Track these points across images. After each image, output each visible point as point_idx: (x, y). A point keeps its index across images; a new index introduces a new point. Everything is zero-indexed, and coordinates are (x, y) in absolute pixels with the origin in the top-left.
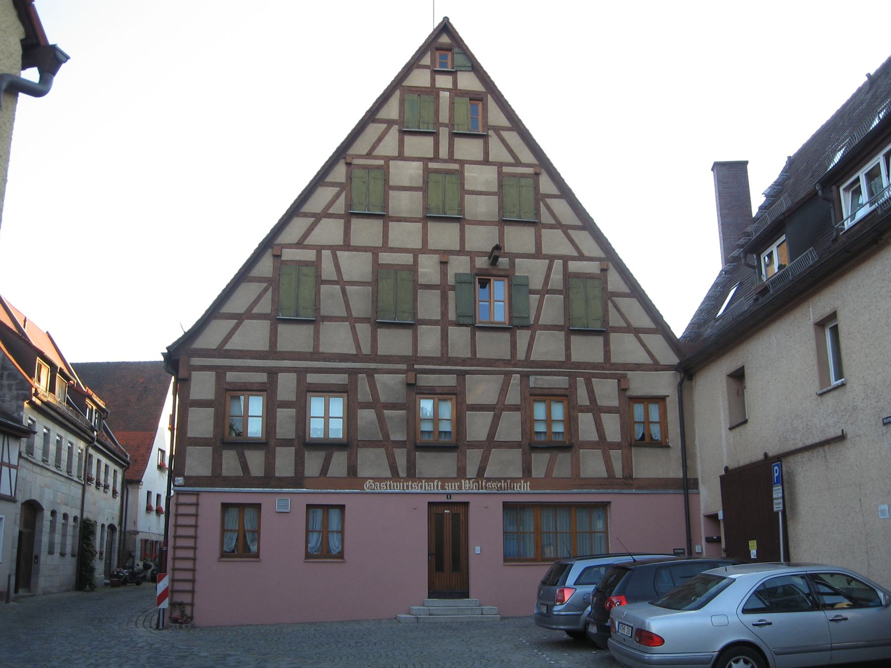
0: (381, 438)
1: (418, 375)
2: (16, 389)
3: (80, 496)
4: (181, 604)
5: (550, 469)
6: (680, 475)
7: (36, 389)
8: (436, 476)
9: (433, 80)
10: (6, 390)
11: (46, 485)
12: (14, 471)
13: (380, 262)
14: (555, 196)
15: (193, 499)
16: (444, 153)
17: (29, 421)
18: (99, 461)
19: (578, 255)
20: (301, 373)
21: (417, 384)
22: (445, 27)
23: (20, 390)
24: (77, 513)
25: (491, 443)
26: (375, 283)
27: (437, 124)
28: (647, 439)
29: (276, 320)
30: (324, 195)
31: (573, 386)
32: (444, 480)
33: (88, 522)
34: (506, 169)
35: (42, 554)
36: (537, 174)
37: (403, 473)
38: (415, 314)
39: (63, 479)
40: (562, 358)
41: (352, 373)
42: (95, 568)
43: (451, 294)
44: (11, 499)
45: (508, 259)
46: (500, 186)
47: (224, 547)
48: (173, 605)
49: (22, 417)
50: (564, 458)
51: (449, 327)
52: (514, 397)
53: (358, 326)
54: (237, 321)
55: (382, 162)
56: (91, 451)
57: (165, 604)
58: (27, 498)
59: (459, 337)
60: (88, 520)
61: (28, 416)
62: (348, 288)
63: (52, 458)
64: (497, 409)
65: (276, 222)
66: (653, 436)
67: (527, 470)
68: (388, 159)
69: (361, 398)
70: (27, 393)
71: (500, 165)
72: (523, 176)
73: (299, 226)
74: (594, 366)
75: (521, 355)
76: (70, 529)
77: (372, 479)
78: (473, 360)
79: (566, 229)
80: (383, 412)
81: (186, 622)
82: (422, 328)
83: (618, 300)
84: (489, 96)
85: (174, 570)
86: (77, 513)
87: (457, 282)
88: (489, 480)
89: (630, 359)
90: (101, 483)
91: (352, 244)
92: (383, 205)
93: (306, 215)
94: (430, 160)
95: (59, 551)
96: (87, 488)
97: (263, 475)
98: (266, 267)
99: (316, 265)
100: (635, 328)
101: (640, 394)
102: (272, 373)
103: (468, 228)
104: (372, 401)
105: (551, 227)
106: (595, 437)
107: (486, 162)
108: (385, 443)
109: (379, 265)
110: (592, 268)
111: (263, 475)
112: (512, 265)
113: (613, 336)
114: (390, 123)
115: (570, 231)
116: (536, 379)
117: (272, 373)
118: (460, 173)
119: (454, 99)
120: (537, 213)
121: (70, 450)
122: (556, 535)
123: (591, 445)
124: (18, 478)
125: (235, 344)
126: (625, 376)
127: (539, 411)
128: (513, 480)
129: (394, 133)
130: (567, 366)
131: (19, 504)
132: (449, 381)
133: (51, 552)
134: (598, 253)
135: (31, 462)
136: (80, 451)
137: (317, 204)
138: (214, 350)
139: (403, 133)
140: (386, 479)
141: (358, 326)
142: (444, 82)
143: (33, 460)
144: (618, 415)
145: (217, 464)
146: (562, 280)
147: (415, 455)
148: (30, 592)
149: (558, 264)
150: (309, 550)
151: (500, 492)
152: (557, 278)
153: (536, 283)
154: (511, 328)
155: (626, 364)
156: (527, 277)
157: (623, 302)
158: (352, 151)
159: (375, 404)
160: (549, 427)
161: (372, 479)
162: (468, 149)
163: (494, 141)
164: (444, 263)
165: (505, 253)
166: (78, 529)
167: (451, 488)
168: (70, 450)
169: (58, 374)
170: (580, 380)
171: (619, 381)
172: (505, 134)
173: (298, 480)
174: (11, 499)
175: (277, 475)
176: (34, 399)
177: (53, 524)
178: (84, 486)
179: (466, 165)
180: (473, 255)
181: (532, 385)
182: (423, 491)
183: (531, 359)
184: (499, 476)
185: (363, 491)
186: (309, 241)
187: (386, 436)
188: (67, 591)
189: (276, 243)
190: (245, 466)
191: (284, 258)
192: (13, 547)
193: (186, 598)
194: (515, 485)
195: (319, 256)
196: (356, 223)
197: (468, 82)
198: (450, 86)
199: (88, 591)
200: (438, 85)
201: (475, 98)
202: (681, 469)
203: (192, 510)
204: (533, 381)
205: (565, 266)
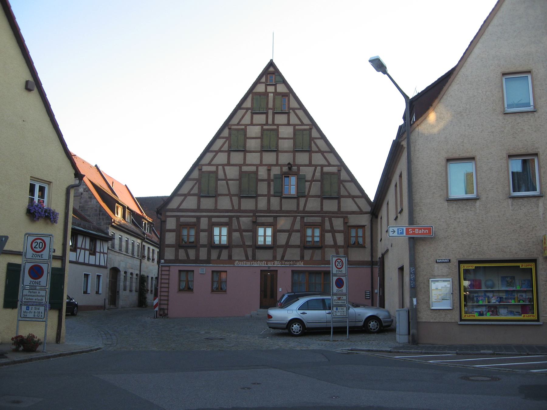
0: (241, 243)
1: (257, 218)
2: (106, 220)
3: (139, 265)
4: (163, 309)
5: (312, 257)
6: (370, 259)
7: (114, 220)
8: (264, 259)
9: (266, 89)
10: (101, 220)
11: (121, 261)
12: (106, 255)
13: (242, 171)
14: (318, 138)
15: (167, 268)
16: (270, 121)
17: (112, 233)
18: (149, 248)
19: (328, 164)
20: (210, 217)
21: (257, 222)
22: (271, 64)
23: (107, 220)
24: (138, 272)
25: (287, 246)
26: (240, 179)
27: (268, 109)
28: (356, 244)
29: (200, 196)
30: (220, 142)
31: (323, 222)
32: (267, 261)
33: (143, 276)
34: (297, 127)
35: (120, 290)
36: (311, 129)
37: (250, 258)
38: (256, 192)
39: (130, 257)
40: (319, 210)
41: (230, 217)
42: (146, 297)
43: (272, 183)
44: (105, 267)
45: (297, 167)
46: (294, 134)
47: (181, 287)
48: (160, 309)
49: (108, 232)
50: (318, 252)
51: (271, 197)
52: (297, 226)
53: (233, 198)
54: (184, 197)
55: (243, 127)
56: (144, 243)
57: (157, 309)
58: (112, 266)
59: (275, 201)
60: (143, 275)
61: (111, 231)
62: (229, 182)
63: (124, 248)
64: (290, 232)
65: (199, 155)
66: (360, 242)
67: (302, 257)
68: (246, 125)
69: (234, 227)
70: (110, 221)
71: (295, 125)
72: (305, 130)
73: (209, 156)
74: (333, 213)
75: (301, 208)
76: (134, 280)
78: (281, 211)
79: (322, 153)
80: (242, 234)
81: (165, 316)
82: (259, 198)
83: (345, 184)
84: (291, 94)
85: (160, 296)
86: (138, 272)
87: (274, 178)
88: (286, 261)
89: (349, 209)
90: (150, 258)
91: (231, 163)
92: (244, 146)
93: (212, 151)
94: (264, 125)
95: (129, 289)
96: (143, 261)
97: (195, 259)
98: (195, 175)
99: (216, 172)
100: (352, 196)
101: (353, 225)
102: (198, 218)
103: (280, 154)
104: (238, 229)
105: (316, 152)
106: (332, 243)
107: (288, 124)
108: (243, 246)
109: (242, 171)
110: (334, 169)
111: (195, 259)
112: (299, 170)
113: (342, 200)
114: (247, 109)
115: (325, 154)
116: (307, 219)
117: (198, 218)
118: (277, 130)
119: (275, 97)
120: (310, 146)
121: (133, 244)
122: (163, 283)
123: (330, 247)
124: (108, 258)
125: (184, 206)
126: (347, 217)
127: (309, 232)
128: (296, 261)
129: (249, 113)
130: (321, 213)
131: (109, 269)
132: (271, 220)
133: (125, 289)
134: (337, 163)
135: (113, 251)
136: (138, 244)
137: (216, 147)
138: (175, 209)
139: (253, 114)
140: (244, 260)
141: (233, 198)
142: (271, 89)
143: (114, 250)
144: (343, 234)
145: (177, 255)
146: (320, 176)
147: (256, 251)
148: (115, 306)
149: (319, 168)
150: (213, 288)
151: (291, 266)
152: (318, 175)
153: (309, 177)
154: (297, 198)
155: (348, 211)
156: (305, 175)
157: (347, 185)
158: (231, 123)
159: (240, 230)
160: (313, 239)
162: (281, 119)
163: (292, 115)
164: (269, 170)
165: (295, 165)
166: (139, 279)
167: (270, 264)
168: (133, 244)
169: (127, 209)
170: (327, 219)
171: (344, 219)
172: (297, 111)
173: (208, 261)
174: (105, 267)
175: (200, 259)
176: (113, 224)
177: (125, 277)
178: (141, 260)
179: (279, 126)
180: (281, 166)
181: (305, 221)
182: (259, 265)
183: (306, 210)
184: (290, 259)
185: (234, 265)
186: (213, 163)
187: (244, 243)
188: (134, 307)
189: (200, 164)
190: (187, 255)
191: (203, 170)
192: (106, 288)
193: (165, 307)
194: (297, 263)
195: (217, 169)
196: (232, 154)
197: (281, 88)
198: (274, 91)
199: (144, 308)
200: (268, 91)
201: (284, 95)
202: (370, 257)
203: (167, 273)
204: (306, 220)
205: (322, 169)
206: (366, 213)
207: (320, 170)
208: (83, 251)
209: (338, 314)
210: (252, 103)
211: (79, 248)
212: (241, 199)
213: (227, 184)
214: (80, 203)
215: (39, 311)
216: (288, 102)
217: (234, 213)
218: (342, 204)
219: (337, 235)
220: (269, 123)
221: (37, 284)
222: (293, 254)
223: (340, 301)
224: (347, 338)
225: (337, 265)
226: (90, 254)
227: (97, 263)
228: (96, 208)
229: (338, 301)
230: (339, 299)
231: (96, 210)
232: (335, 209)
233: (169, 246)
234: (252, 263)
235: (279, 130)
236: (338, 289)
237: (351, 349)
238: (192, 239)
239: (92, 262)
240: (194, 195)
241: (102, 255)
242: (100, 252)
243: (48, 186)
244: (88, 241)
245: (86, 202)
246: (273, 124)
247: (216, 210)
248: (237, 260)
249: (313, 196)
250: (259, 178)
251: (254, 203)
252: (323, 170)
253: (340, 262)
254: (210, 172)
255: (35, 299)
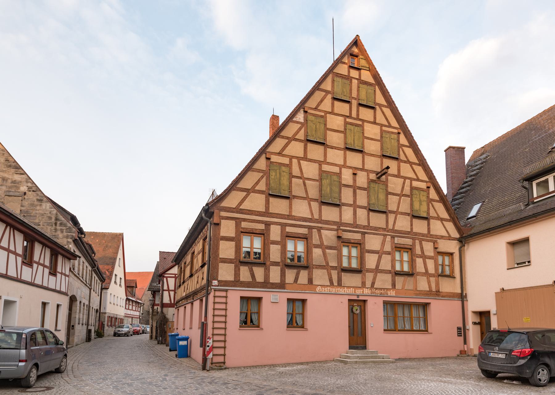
5: (404, 285)
10: (59, 232)
12: (67, 278)
15: (224, 294)
16: (354, 114)
25: (377, 270)
34: (384, 128)
37: (335, 284)
41: (310, 228)
52: (388, 247)
55: (323, 114)
62: (307, 182)
67: (394, 285)
68: (327, 112)
71: (382, 125)
74: (423, 235)
75: (390, 227)
78: (368, 227)
82: (344, 208)
97: (263, 281)
99: (289, 166)
105: (405, 162)
106: (423, 270)
107: (374, 123)
108: (326, 267)
113: (432, 221)
116: (398, 239)
118: (362, 126)
145: (237, 273)
149: (408, 181)
167: (359, 292)
174: (65, 294)
175: (271, 281)
181: (396, 242)
184: (381, 287)
185: (315, 292)
187: (327, 263)
204: (397, 240)
206: (454, 239)
207: (409, 184)
208: (41, 268)
210: (333, 86)
211: (36, 263)
212: (322, 206)
213: (305, 184)
214: (22, 206)
222: (384, 281)
226: (50, 273)
227: (58, 289)
228: (49, 215)
231: (50, 218)
233: (225, 261)
234: (338, 290)
239: (52, 286)
241: (63, 277)
242: (62, 273)
244: (48, 253)
245: (32, 205)
247: (289, 217)
248: (319, 285)
249: (402, 214)
251: (338, 213)
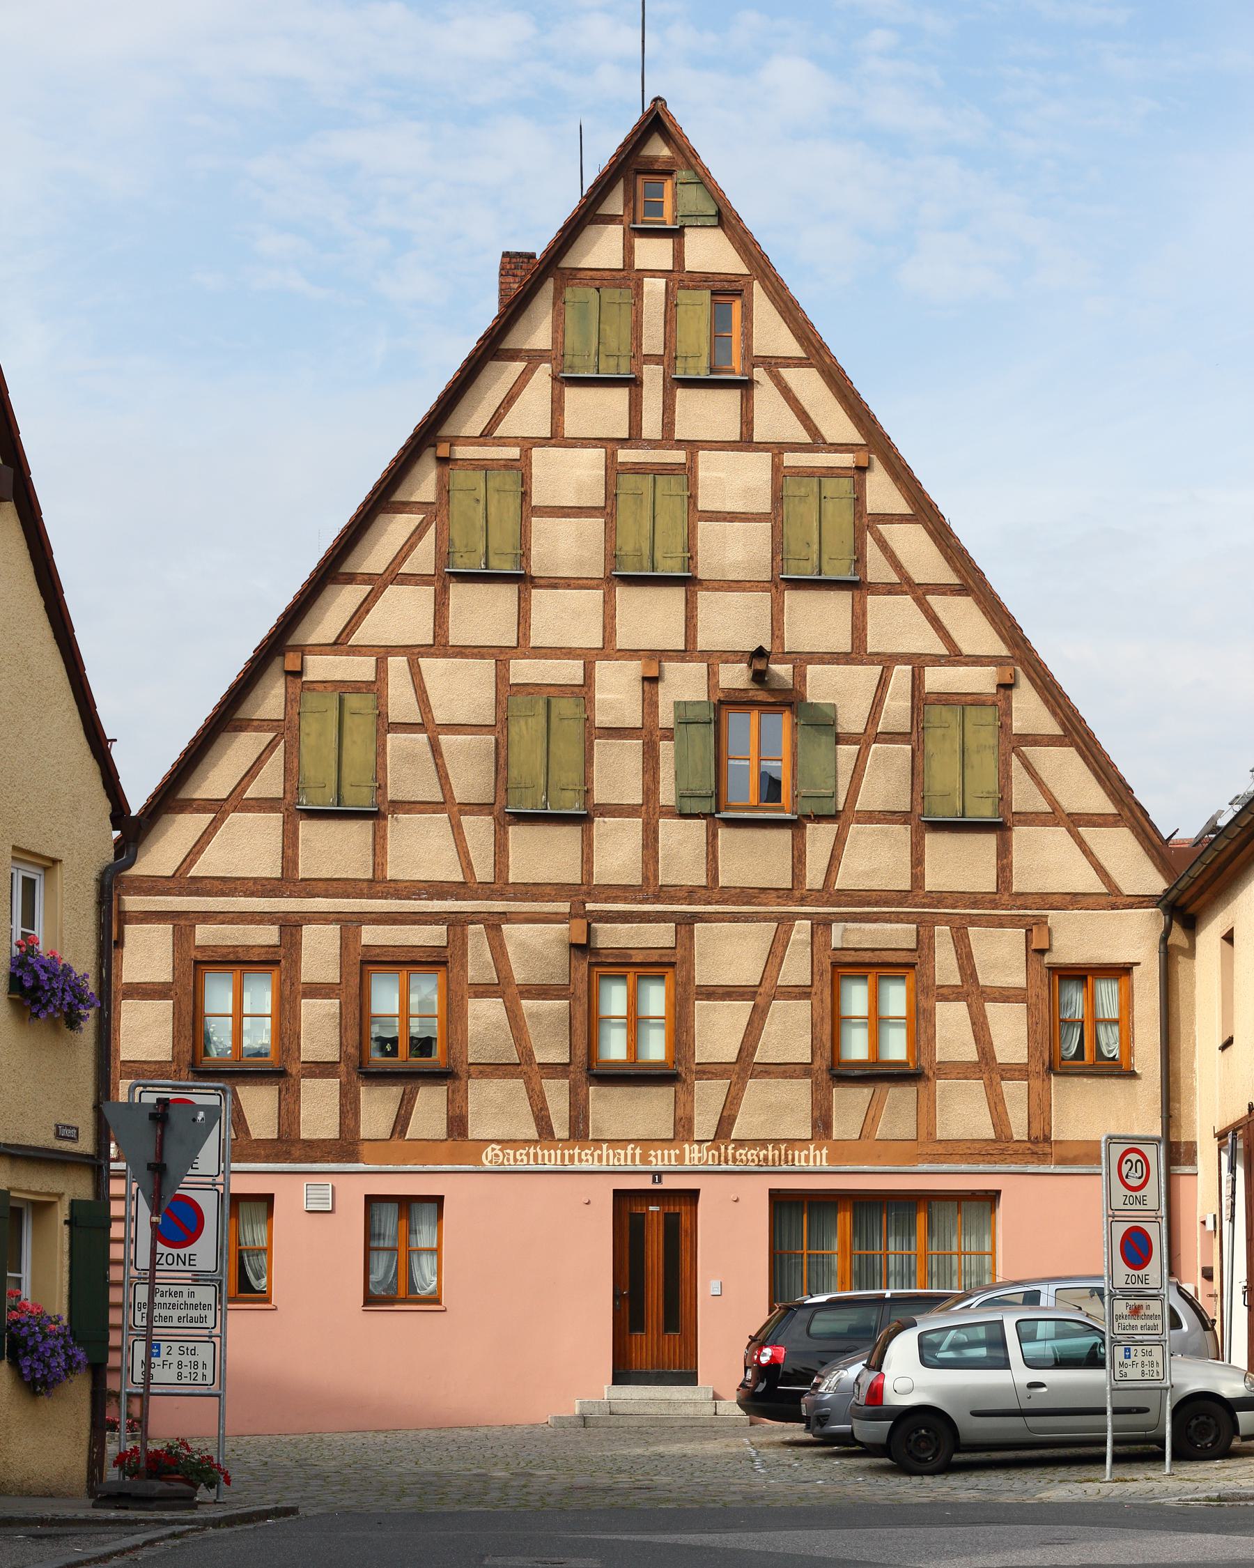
5: (870, 1120)
9: (629, 250)
16: (651, 426)
20: (349, 923)
26: (501, 726)
27: (640, 358)
31: (924, 945)
32: (646, 1143)
34: (790, 459)
37: (561, 1131)
41: (456, 922)
43: (666, 749)
46: (778, 498)
50: (900, 1097)
51: (661, 820)
52: (796, 969)
55: (514, 453)
62: (443, 738)
67: (822, 1124)
68: (528, 444)
69: (473, 975)
71: (778, 448)
72: (831, 472)
74: (975, 899)
75: (814, 878)
77: (498, 1142)
78: (712, 890)
94: (622, 442)
99: (376, 688)
100: (1069, 815)
102: (291, 926)
103: (703, 597)
106: (970, 1053)
107: (746, 443)
110: (981, 680)
112: (800, 676)
113: (1020, 834)
116: (846, 930)
118: (688, 472)
120: (859, 560)
123: (962, 1071)
125: (209, 865)
126: (1041, 921)
132: (660, 936)
139: (563, 381)
152: (897, 708)
153: (852, 719)
161: (498, 1142)
163: (766, 396)
164: (651, 681)
170: (942, 932)
171: (1029, 931)
172: (789, 374)
175: (304, 1135)
180: (713, 659)
181: (836, 942)
187: (527, 1054)
194: (797, 1153)
204: (838, 935)
209: (1134, 1373)
210: (558, 329)
215: (193, 1359)
216: (744, 327)
217: (474, 899)
218: (1018, 858)
219: (993, 1010)
220: (644, 436)
221: (184, 1264)
223: (1139, 1323)
224: (1167, 1471)
225: (1127, 1177)
229: (1133, 1322)
230: (1135, 1312)
232: (986, 882)
234: (572, 1158)
235: (696, 472)
236: (1132, 1272)
237: (1219, 1496)
238: (259, 1036)
240: (265, 805)
243: (42, 877)
246: (668, 440)
248: (492, 1141)
249: (871, 817)
250: (601, 719)
252: (922, 682)
253: (1139, 1163)
254: (344, 688)
255: (179, 1318)
